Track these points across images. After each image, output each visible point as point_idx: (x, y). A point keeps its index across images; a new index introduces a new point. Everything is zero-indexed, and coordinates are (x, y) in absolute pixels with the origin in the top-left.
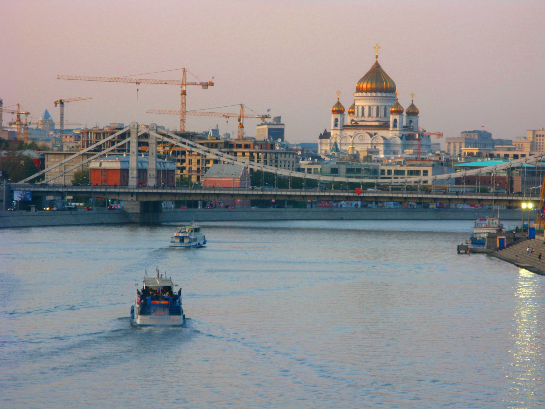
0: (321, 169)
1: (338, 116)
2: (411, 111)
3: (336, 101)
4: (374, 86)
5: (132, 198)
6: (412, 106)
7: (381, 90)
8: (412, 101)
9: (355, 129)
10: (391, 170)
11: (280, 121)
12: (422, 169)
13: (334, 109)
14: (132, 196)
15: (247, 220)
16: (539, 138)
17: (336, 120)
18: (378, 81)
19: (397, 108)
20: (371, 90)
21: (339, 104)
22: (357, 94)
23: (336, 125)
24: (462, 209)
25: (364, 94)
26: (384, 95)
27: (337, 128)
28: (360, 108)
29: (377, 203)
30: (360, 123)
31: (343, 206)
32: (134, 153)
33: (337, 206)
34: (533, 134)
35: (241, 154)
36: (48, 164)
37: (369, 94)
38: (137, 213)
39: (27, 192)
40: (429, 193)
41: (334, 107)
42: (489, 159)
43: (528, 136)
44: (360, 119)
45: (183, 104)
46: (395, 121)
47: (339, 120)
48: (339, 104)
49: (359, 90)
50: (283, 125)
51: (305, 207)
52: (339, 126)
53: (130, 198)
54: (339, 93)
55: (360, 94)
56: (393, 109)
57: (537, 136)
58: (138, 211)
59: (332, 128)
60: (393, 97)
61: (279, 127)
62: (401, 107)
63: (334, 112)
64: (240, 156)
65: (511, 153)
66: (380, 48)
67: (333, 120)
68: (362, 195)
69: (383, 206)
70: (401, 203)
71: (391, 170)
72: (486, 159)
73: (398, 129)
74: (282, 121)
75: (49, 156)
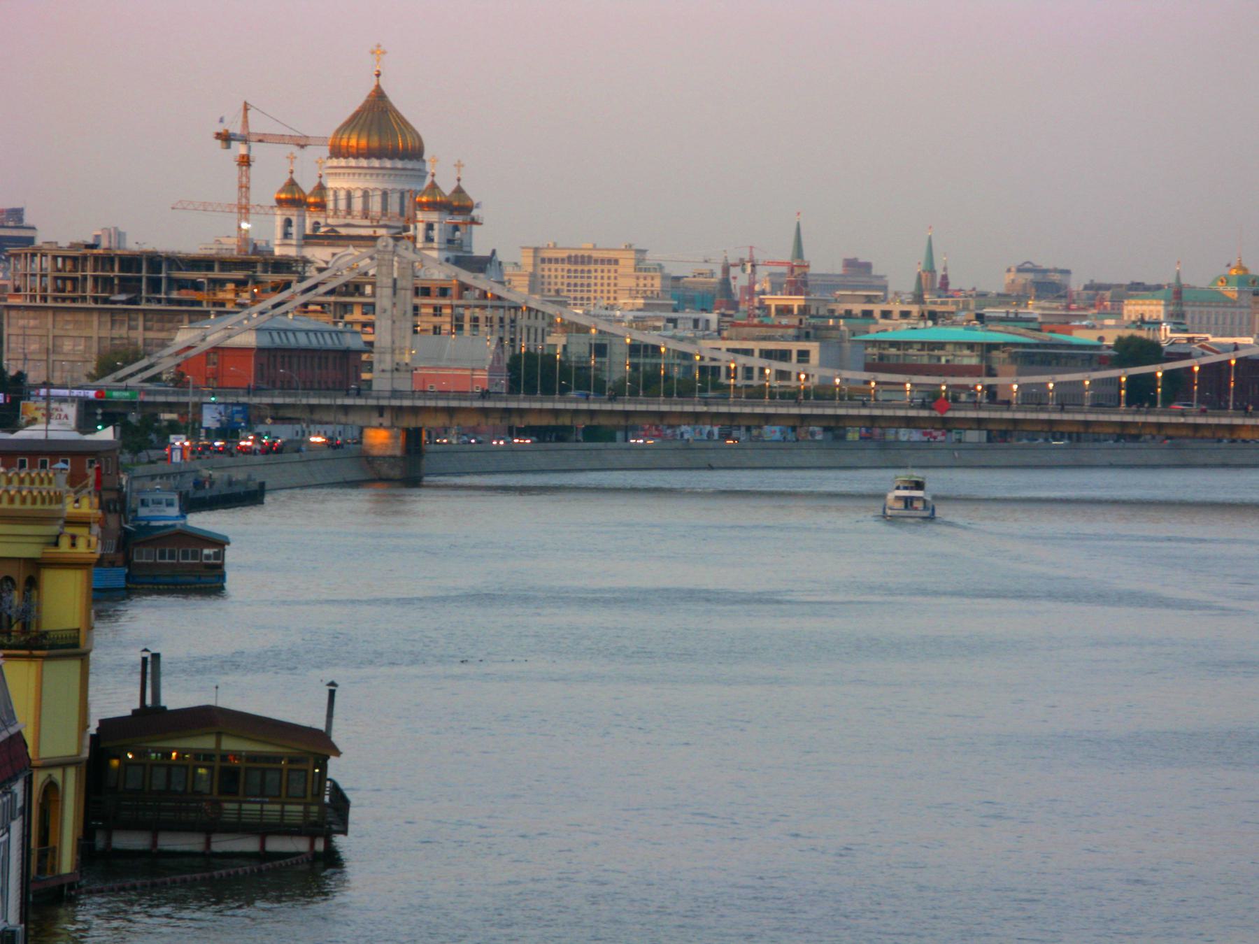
0: (565, 347)
1: (293, 214)
2: (456, 203)
3: (285, 179)
4: (375, 143)
5: (381, 420)
6: (459, 191)
7: (394, 154)
8: (459, 180)
9: (329, 245)
10: (790, 351)
11: (21, 220)
12: (795, 347)
13: (283, 196)
14: (381, 415)
15: (542, 471)
16: (546, 266)
17: (288, 223)
18: (380, 132)
19: (435, 195)
20: (368, 154)
21: (292, 184)
22: (335, 162)
23: (286, 235)
24: (908, 441)
25: (352, 162)
26: (399, 164)
27: (288, 241)
28: (342, 195)
29: (748, 429)
30: (343, 231)
31: (686, 436)
32: (385, 311)
33: (674, 435)
34: (535, 257)
35: (431, 311)
36: (11, 331)
37: (363, 162)
38: (394, 457)
39: (235, 408)
40: (1042, 410)
41: (281, 191)
42: (930, 323)
43: (521, 261)
44: (341, 221)
45: (244, 187)
46: (430, 227)
47: (294, 223)
48: (292, 184)
49: (336, 152)
50: (33, 228)
51: (613, 439)
52: (294, 236)
53: (375, 421)
54: (459, 165)
55: (342, 162)
56: (424, 199)
57: (543, 261)
58: (398, 452)
59: (277, 242)
60: (419, 170)
61: (23, 233)
62: (300, 190)
63: (280, 202)
64: (427, 314)
65: (877, 309)
66: (384, 53)
67: (279, 221)
68: (950, 414)
69: (760, 435)
70: (794, 429)
71: (790, 351)
72: (922, 324)
73: (435, 245)
74: (27, 221)
75: (13, 313)
